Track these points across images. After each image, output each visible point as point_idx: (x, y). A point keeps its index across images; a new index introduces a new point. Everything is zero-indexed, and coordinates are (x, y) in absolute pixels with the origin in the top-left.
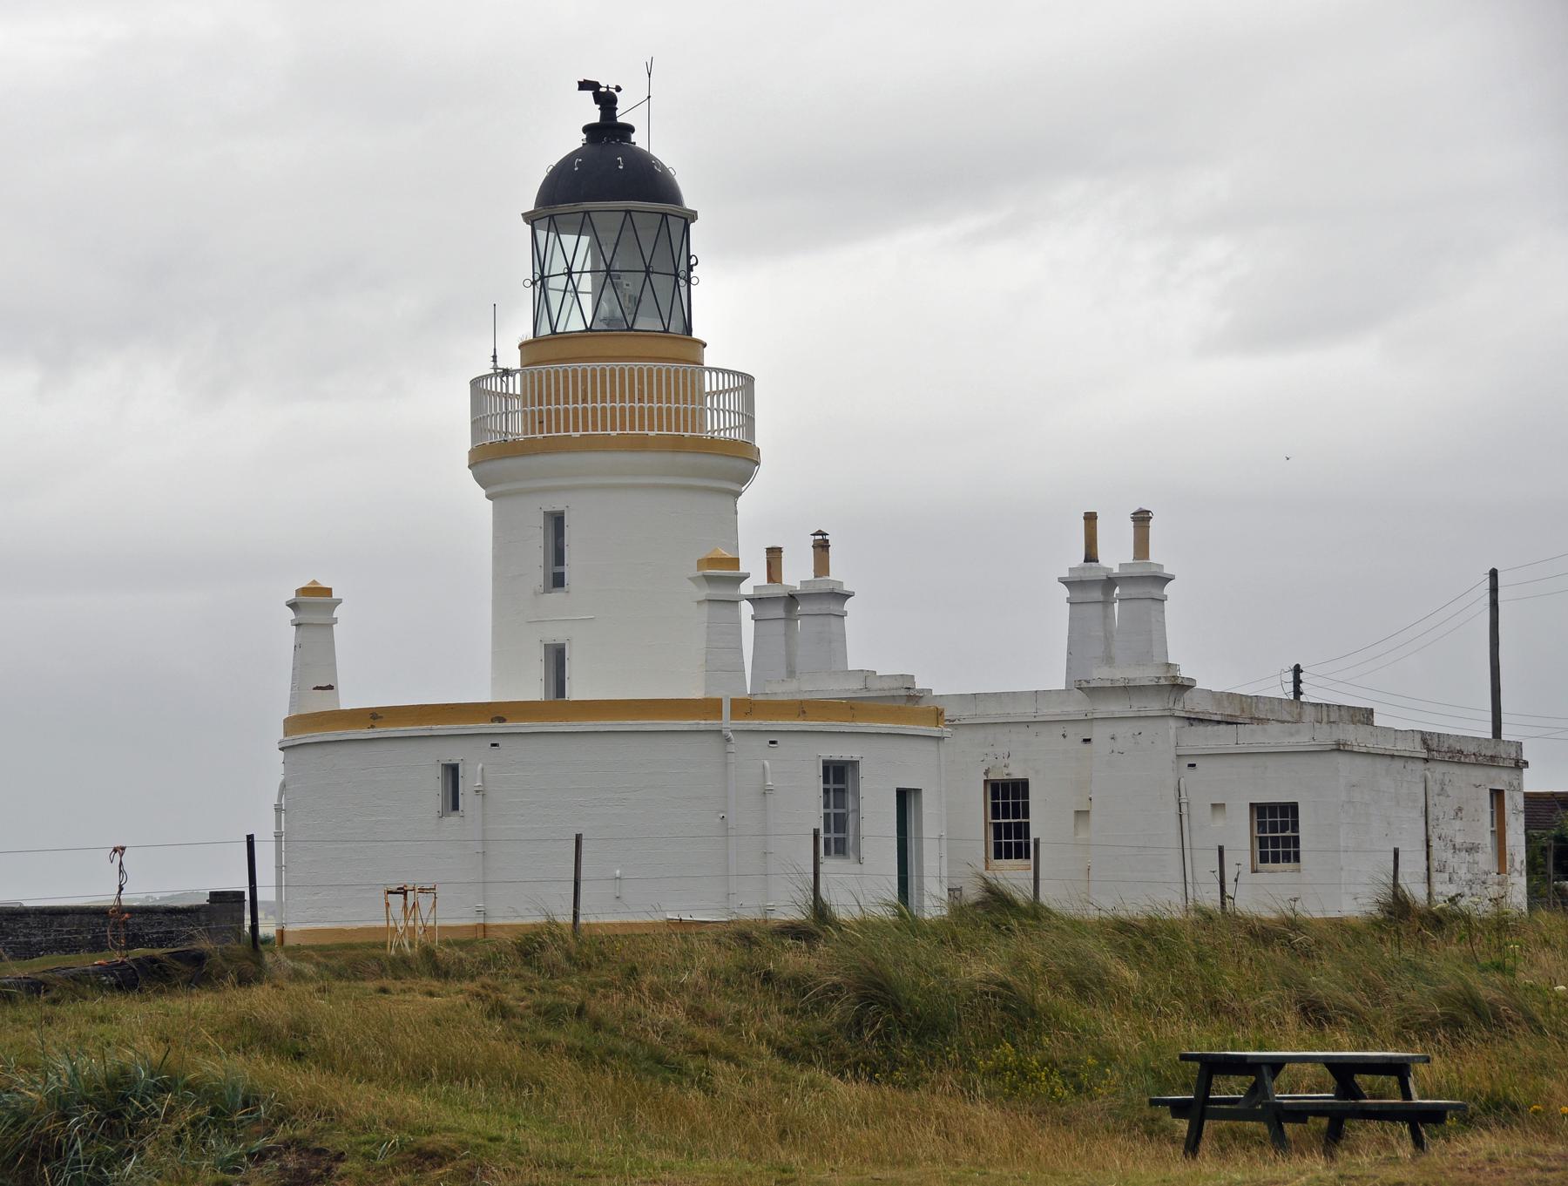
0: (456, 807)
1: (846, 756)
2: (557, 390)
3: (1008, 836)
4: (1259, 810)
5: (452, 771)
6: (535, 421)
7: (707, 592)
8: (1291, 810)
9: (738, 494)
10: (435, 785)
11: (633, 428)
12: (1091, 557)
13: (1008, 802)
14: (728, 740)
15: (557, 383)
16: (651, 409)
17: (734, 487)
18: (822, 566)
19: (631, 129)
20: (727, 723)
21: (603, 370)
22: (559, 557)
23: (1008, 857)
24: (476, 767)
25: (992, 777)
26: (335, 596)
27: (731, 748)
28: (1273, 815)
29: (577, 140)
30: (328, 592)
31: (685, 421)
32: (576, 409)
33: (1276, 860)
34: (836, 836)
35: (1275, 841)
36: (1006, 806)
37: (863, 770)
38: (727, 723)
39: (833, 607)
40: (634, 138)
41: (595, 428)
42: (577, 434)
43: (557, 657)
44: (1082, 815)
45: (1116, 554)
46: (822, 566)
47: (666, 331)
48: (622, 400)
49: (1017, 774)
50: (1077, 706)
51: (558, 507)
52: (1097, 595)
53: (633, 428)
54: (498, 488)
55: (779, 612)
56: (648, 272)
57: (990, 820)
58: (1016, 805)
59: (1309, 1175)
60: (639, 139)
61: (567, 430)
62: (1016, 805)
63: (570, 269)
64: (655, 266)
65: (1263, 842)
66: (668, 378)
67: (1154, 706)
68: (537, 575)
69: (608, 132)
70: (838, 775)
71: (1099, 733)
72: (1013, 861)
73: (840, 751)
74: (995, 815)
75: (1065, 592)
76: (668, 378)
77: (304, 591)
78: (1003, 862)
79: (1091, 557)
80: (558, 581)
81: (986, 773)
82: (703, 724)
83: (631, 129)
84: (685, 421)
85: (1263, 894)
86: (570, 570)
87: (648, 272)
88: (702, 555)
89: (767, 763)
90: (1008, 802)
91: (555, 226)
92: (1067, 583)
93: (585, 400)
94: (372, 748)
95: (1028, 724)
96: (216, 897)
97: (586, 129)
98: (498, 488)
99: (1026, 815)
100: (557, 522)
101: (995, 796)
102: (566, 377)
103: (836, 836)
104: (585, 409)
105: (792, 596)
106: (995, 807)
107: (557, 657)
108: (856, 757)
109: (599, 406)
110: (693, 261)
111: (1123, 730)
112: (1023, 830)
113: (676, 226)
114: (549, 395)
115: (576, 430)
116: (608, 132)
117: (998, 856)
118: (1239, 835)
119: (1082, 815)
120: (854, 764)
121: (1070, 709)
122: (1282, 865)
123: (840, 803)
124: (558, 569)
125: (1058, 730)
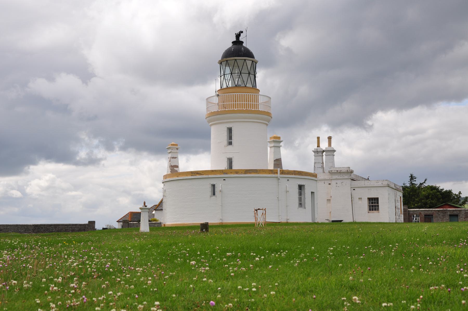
0: (214, 194)
4: (369, 199)
5: (214, 186)
8: (377, 199)
9: (334, 155)
10: (209, 189)
12: (318, 146)
15: (233, 98)
17: (267, 123)
18: (330, 144)
19: (243, 42)
20: (279, 175)
22: (230, 138)
24: (220, 185)
27: (279, 181)
28: (372, 200)
33: (373, 210)
35: (373, 206)
37: (306, 187)
38: (279, 175)
43: (230, 161)
44: (329, 200)
45: (324, 145)
46: (330, 144)
48: (244, 101)
52: (320, 154)
56: (249, 74)
59: (404, 278)
61: (242, 108)
65: (370, 206)
67: (346, 177)
68: (225, 141)
70: (301, 187)
71: (333, 183)
73: (302, 183)
75: (313, 153)
79: (318, 146)
80: (230, 143)
82: (273, 175)
83: (243, 42)
85: (374, 217)
86: (234, 141)
87: (241, 73)
91: (227, 64)
92: (314, 152)
94: (177, 182)
96: (89, 222)
97: (233, 43)
100: (230, 130)
107: (230, 161)
111: (339, 182)
113: (254, 63)
116: (238, 42)
118: (365, 204)
119: (329, 200)
120: (304, 186)
121: (326, 177)
122: (374, 211)
124: (230, 141)
125: (323, 182)
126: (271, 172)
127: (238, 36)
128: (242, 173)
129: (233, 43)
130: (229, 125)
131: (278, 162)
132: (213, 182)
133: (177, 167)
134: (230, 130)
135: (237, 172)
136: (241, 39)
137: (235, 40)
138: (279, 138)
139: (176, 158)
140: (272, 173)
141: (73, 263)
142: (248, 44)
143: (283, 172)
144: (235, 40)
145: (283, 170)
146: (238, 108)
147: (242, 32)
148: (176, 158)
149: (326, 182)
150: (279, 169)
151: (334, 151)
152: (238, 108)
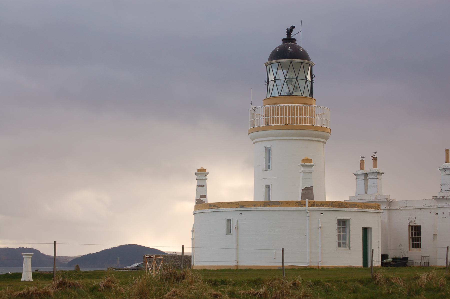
1: (345, 218)
2: (273, 112)
3: (415, 241)
5: (229, 221)
6: (266, 121)
7: (302, 169)
8: (230, 220)
11: (300, 123)
13: (415, 230)
14: (308, 213)
16: (300, 118)
17: (324, 140)
18: (375, 166)
19: (295, 40)
21: (283, 106)
22: (268, 159)
23: (416, 247)
25: (411, 224)
26: (207, 171)
29: (280, 43)
30: (205, 170)
31: (307, 121)
32: (276, 118)
34: (342, 242)
36: (415, 232)
37: (351, 222)
38: (307, 208)
39: (379, 176)
40: (296, 42)
41: (310, 124)
42: (273, 125)
46: (375, 166)
47: (302, 96)
49: (418, 223)
50: (434, 204)
51: (269, 146)
53: (300, 123)
54: (255, 141)
55: (363, 178)
57: (410, 237)
58: (418, 232)
60: (298, 43)
61: (292, 123)
62: (418, 232)
63: (275, 79)
64: (298, 78)
66: (307, 109)
69: (289, 39)
71: (440, 212)
72: (417, 249)
73: (343, 216)
74: (412, 235)
76: (307, 109)
77: (198, 170)
78: (414, 249)
80: (269, 167)
81: (409, 223)
82: (300, 208)
83: (295, 40)
84: (307, 121)
87: (297, 79)
88: (303, 158)
89: (320, 220)
90: (415, 230)
93: (294, 115)
95: (421, 209)
97: (282, 40)
98: (255, 141)
99: (420, 236)
100: (268, 150)
101: (412, 230)
102: (283, 108)
103: (342, 242)
104: (276, 118)
105: (366, 173)
106: (412, 233)
108: (348, 218)
109: (282, 116)
110: (313, 76)
112: (419, 240)
114: (271, 114)
115: (273, 124)
116: (289, 39)
117: (413, 247)
123: (344, 231)
124: (269, 164)
125: (429, 211)
126: (297, 204)
127: (289, 32)
128: (260, 206)
129: (282, 40)
130: (268, 144)
131: (308, 192)
132: (229, 216)
133: (205, 197)
134: (268, 150)
135: (277, 203)
136: (293, 35)
137: (285, 36)
138: (311, 161)
139: (203, 186)
140: (299, 206)
141: (299, 280)
142: (302, 42)
143: (313, 204)
144: (285, 36)
145: (314, 202)
146: (297, 123)
147: (294, 27)
148: (203, 186)
149: (432, 211)
150: (307, 201)
151: (382, 173)
152: (297, 123)
